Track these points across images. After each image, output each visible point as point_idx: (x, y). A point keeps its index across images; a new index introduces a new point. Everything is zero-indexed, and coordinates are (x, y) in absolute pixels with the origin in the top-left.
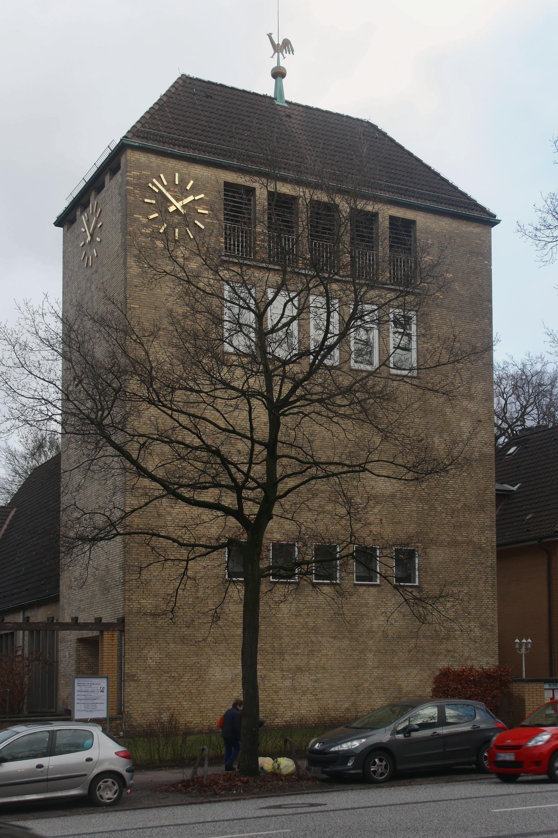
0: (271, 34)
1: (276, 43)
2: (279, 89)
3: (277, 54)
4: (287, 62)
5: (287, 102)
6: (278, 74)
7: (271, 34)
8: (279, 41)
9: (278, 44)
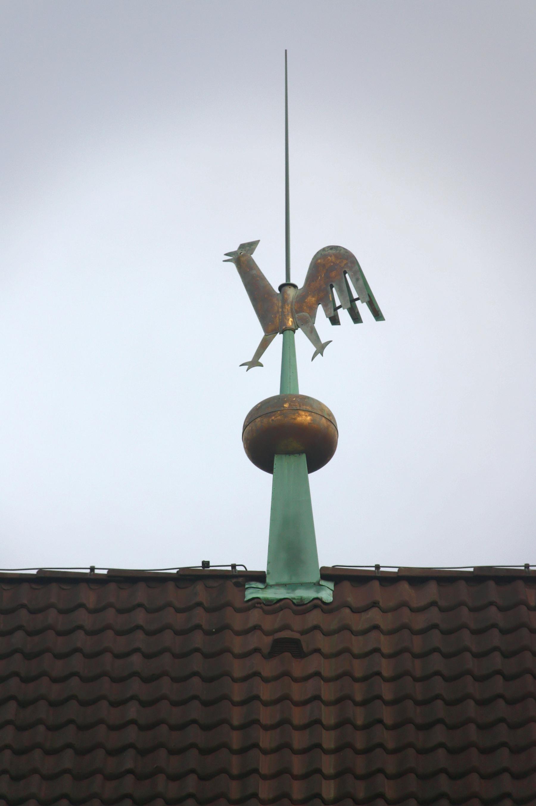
0: (250, 247)
1: (275, 279)
2: (291, 528)
3: (279, 338)
4: (337, 369)
5: (335, 576)
6: (288, 439)
7: (250, 247)
8: (284, 267)
9: (287, 285)
